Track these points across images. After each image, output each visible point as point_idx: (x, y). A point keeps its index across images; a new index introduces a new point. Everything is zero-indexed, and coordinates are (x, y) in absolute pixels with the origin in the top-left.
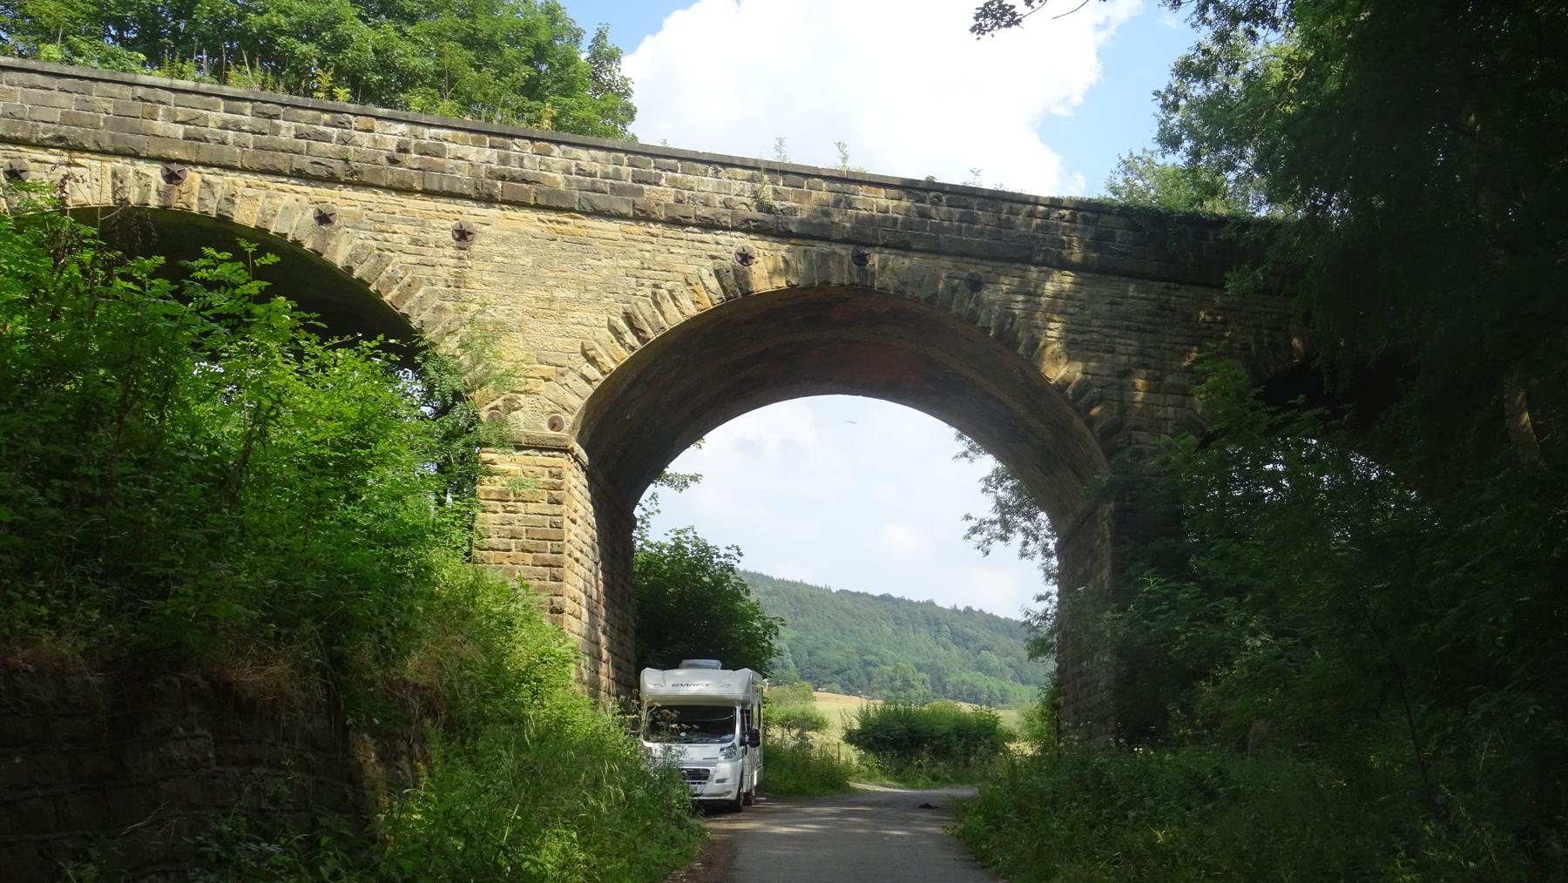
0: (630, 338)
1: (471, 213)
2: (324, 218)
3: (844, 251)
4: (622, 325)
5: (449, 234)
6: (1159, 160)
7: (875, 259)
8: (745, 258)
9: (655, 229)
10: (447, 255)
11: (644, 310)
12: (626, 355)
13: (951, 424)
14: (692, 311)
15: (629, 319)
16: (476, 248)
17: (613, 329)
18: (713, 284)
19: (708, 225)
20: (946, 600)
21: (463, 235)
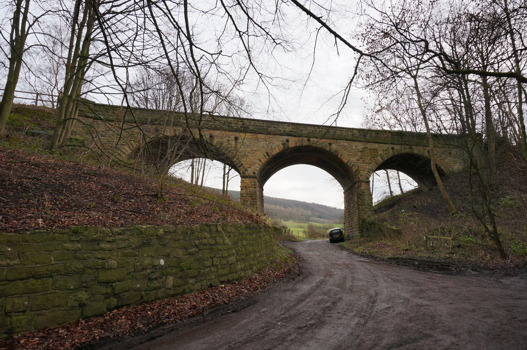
0: (267, 157)
1: (237, 134)
2: (211, 136)
3: (306, 139)
4: (266, 154)
5: (233, 139)
6: (379, 274)
7: (311, 139)
8: (288, 141)
9: (271, 136)
10: (233, 143)
11: (269, 152)
12: (266, 160)
13: (408, 192)
14: (278, 151)
15: (267, 153)
16: (239, 141)
17: (264, 155)
18: (282, 146)
19: (281, 135)
20: (308, 201)
21: (236, 139)
